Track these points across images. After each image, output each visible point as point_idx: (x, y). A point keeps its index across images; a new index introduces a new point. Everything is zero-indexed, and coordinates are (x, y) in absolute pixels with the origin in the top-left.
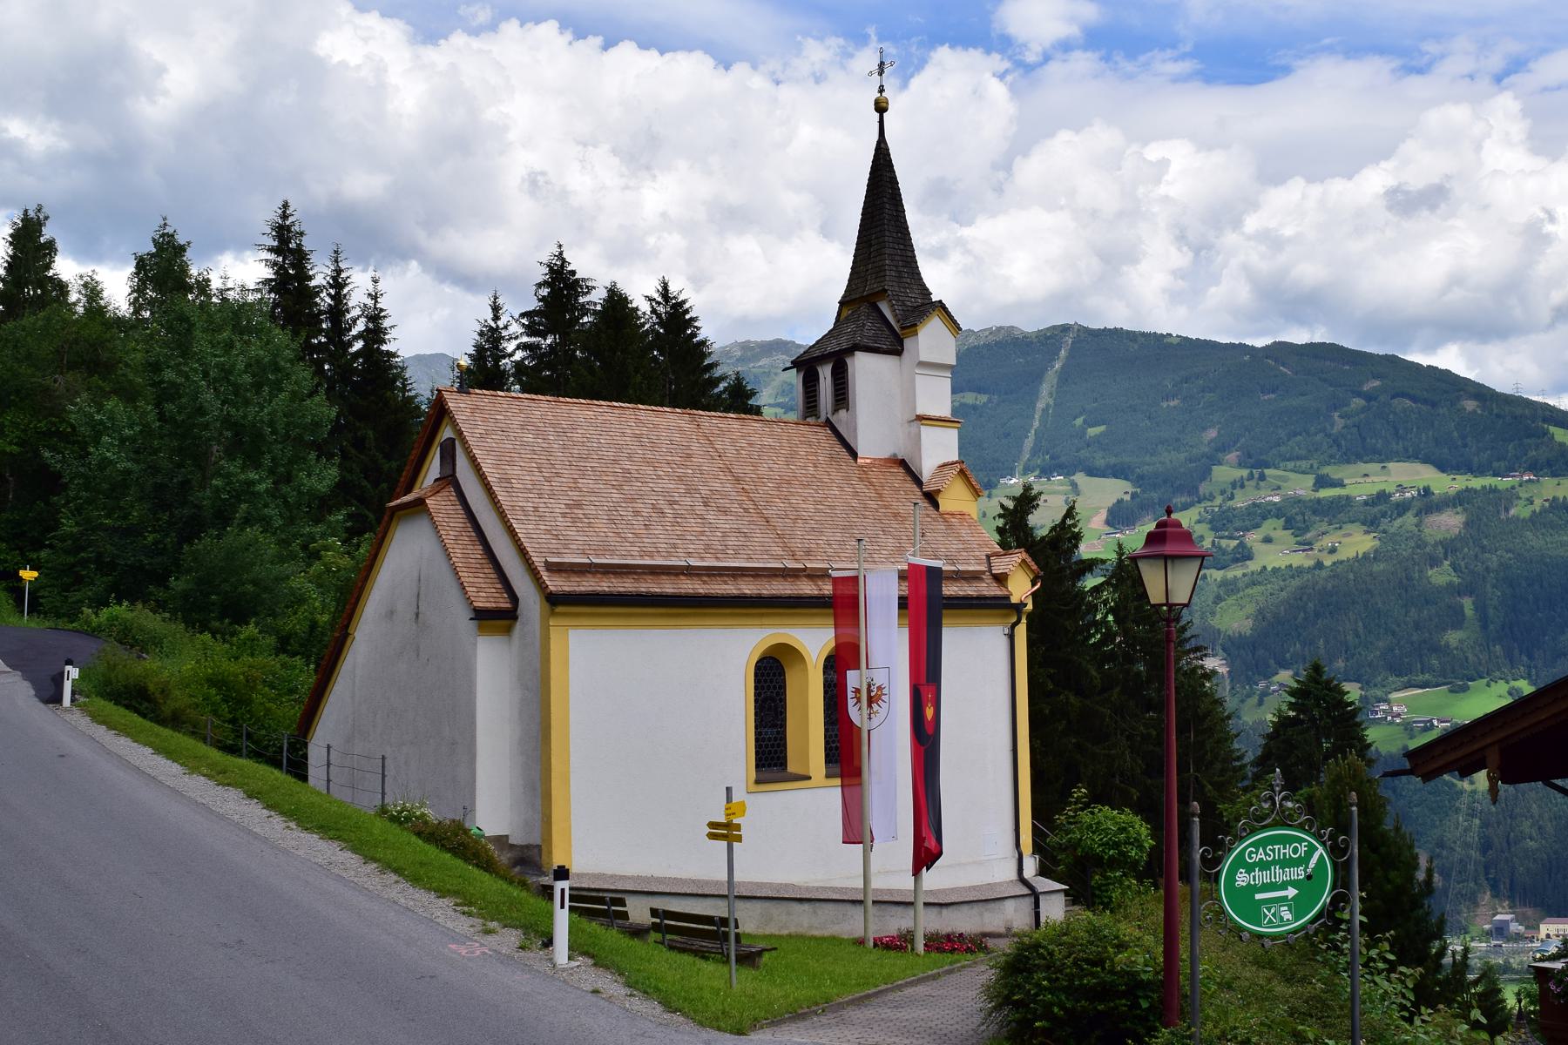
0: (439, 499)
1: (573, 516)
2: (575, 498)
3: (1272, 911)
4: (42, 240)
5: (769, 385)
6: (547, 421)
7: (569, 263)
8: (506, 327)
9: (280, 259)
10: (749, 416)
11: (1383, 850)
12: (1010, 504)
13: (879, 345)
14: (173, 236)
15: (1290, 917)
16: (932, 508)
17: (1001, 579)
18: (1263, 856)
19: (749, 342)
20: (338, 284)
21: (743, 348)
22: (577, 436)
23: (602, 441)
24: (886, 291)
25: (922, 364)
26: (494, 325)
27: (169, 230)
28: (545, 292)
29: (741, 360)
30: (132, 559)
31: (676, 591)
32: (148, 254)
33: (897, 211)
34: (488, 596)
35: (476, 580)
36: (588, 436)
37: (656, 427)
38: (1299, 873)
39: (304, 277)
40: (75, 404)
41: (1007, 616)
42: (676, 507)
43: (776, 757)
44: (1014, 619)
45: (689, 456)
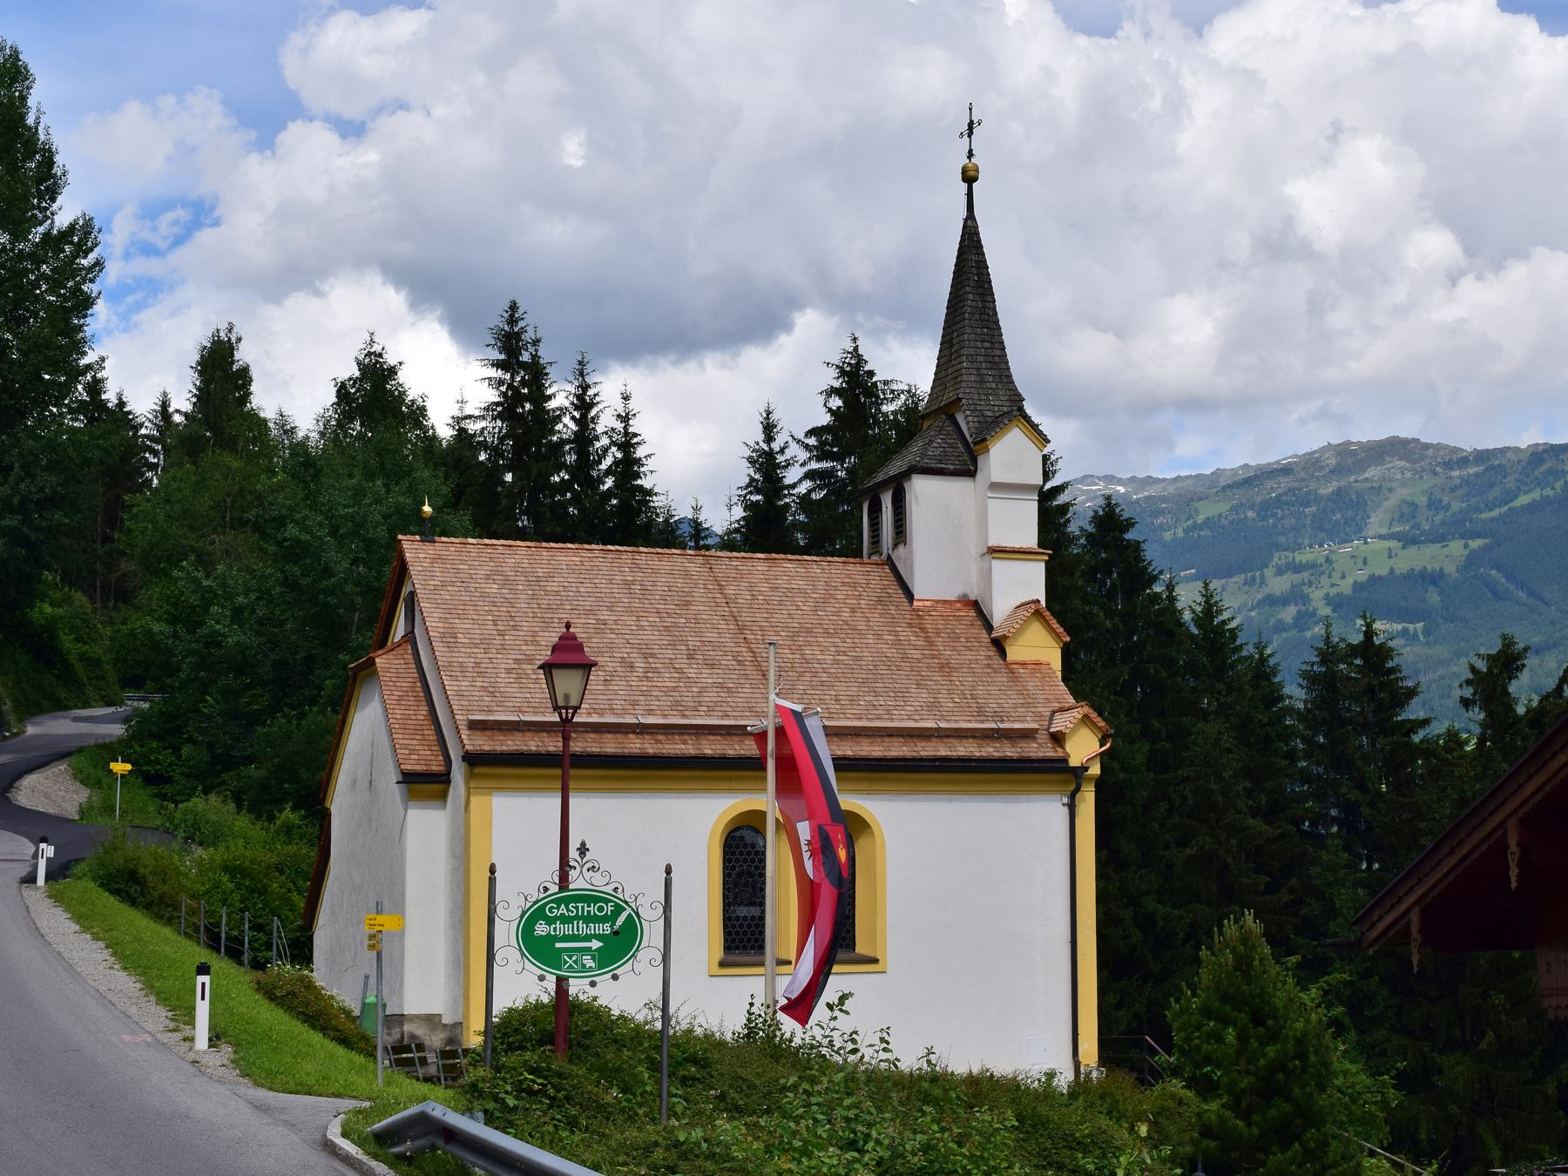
0: (391, 657)
1: (520, 671)
2: (528, 653)
3: (574, 958)
4: (235, 368)
5: (1380, 507)
6: (520, 570)
7: (866, 362)
8: (782, 451)
9: (508, 376)
10: (782, 556)
11: (1270, 1022)
12: (1482, 666)
13: (944, 466)
14: (380, 355)
15: (593, 965)
16: (998, 658)
17: (1058, 739)
18: (565, 912)
19: (1349, 443)
20: (584, 404)
21: (1339, 454)
22: (553, 586)
23: (582, 590)
24: (960, 400)
25: (996, 487)
26: (767, 449)
27: (376, 348)
28: (836, 402)
29: (1337, 471)
30: (250, 749)
31: (618, 751)
32: (350, 379)
33: (983, 301)
34: (423, 758)
35: (412, 742)
36: (566, 584)
37: (654, 572)
38: (606, 929)
39: (540, 397)
40: (182, 569)
41: (1066, 782)
42: (651, 660)
43: (734, 936)
44: (1072, 787)
45: (688, 604)
